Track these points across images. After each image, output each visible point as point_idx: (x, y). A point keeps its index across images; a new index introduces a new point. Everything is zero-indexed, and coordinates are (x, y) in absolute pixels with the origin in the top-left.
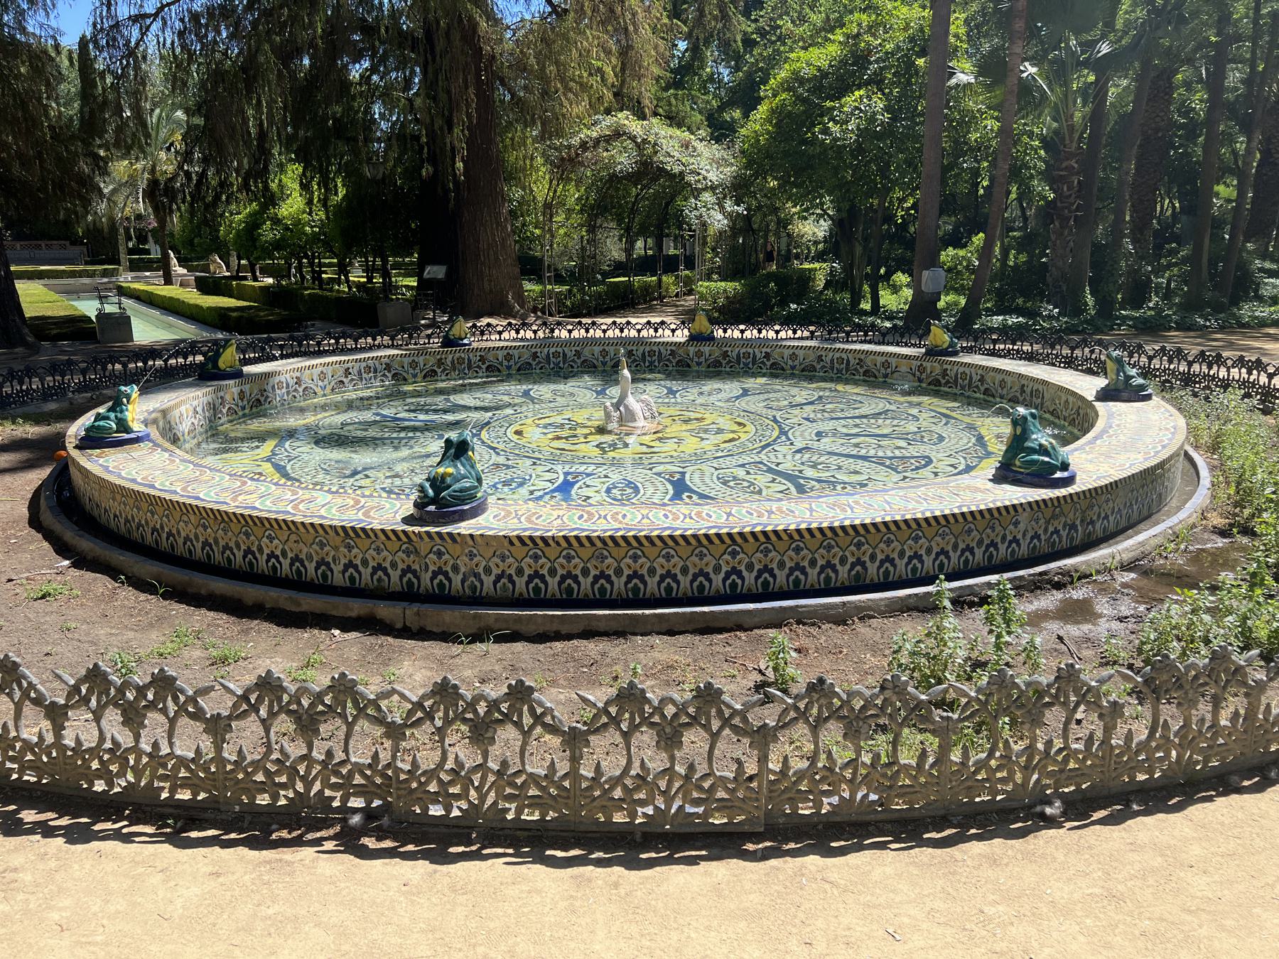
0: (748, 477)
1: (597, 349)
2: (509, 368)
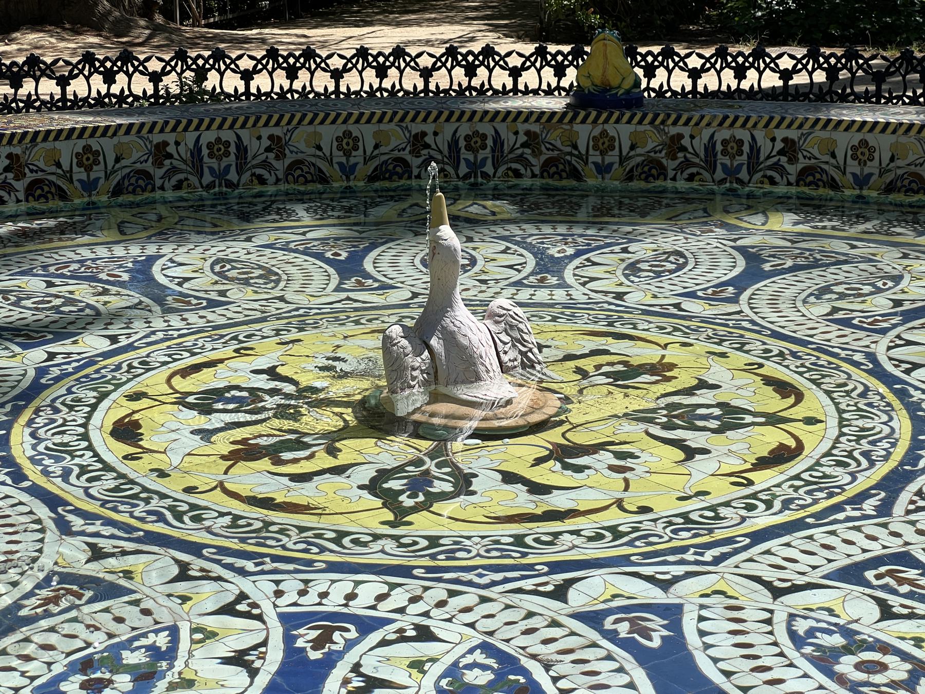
0: (891, 631)
1: (328, 133)
2: (89, 186)
